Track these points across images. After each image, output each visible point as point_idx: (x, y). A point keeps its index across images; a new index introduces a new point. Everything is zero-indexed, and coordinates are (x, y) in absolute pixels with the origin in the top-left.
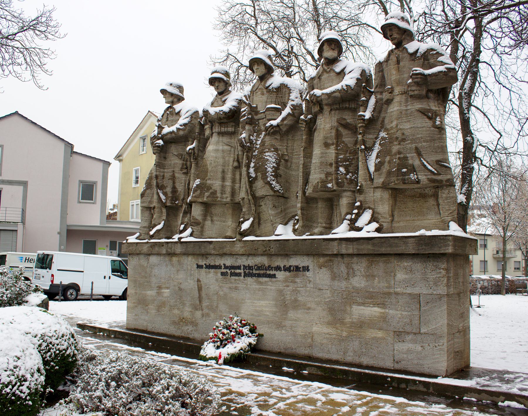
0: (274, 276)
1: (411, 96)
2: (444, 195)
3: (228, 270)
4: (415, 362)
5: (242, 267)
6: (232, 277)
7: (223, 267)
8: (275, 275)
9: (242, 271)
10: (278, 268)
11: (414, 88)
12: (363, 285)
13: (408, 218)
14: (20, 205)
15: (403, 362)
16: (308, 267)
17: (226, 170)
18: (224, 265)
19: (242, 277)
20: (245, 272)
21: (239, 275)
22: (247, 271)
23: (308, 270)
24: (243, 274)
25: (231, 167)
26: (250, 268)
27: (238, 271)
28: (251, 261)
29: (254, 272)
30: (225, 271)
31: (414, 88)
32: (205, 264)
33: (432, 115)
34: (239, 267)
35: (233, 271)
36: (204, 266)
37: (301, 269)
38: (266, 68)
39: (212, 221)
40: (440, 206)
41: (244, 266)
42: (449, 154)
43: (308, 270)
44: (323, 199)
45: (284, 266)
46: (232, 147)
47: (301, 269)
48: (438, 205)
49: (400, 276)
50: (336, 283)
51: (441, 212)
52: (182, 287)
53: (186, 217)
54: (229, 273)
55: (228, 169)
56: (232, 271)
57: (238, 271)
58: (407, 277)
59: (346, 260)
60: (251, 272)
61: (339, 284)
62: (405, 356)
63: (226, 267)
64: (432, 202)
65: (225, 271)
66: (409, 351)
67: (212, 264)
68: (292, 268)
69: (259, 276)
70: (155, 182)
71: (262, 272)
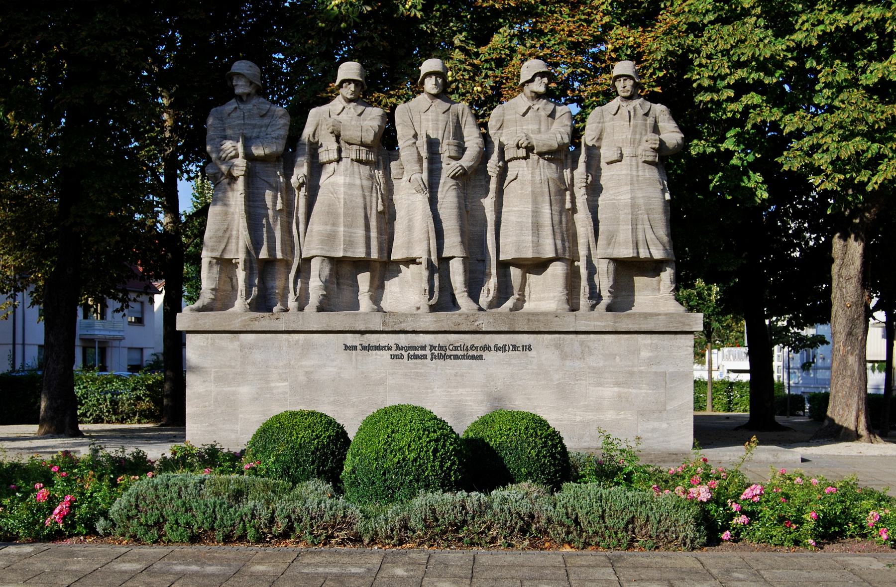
0: (480, 357)
5: (428, 348)
9: (427, 352)
12: (601, 365)
14: (542, 329)
16: (530, 346)
21: (424, 357)
24: (429, 357)
26: (441, 348)
29: (448, 353)
30: (398, 352)
32: (361, 345)
33: (452, 82)
34: (423, 348)
36: (359, 347)
37: (520, 349)
42: (363, 107)
47: (520, 349)
50: (568, 363)
56: (414, 353)
57: (420, 353)
58: (651, 354)
60: (443, 353)
62: (650, 435)
63: (398, 347)
65: (398, 352)
66: (654, 430)
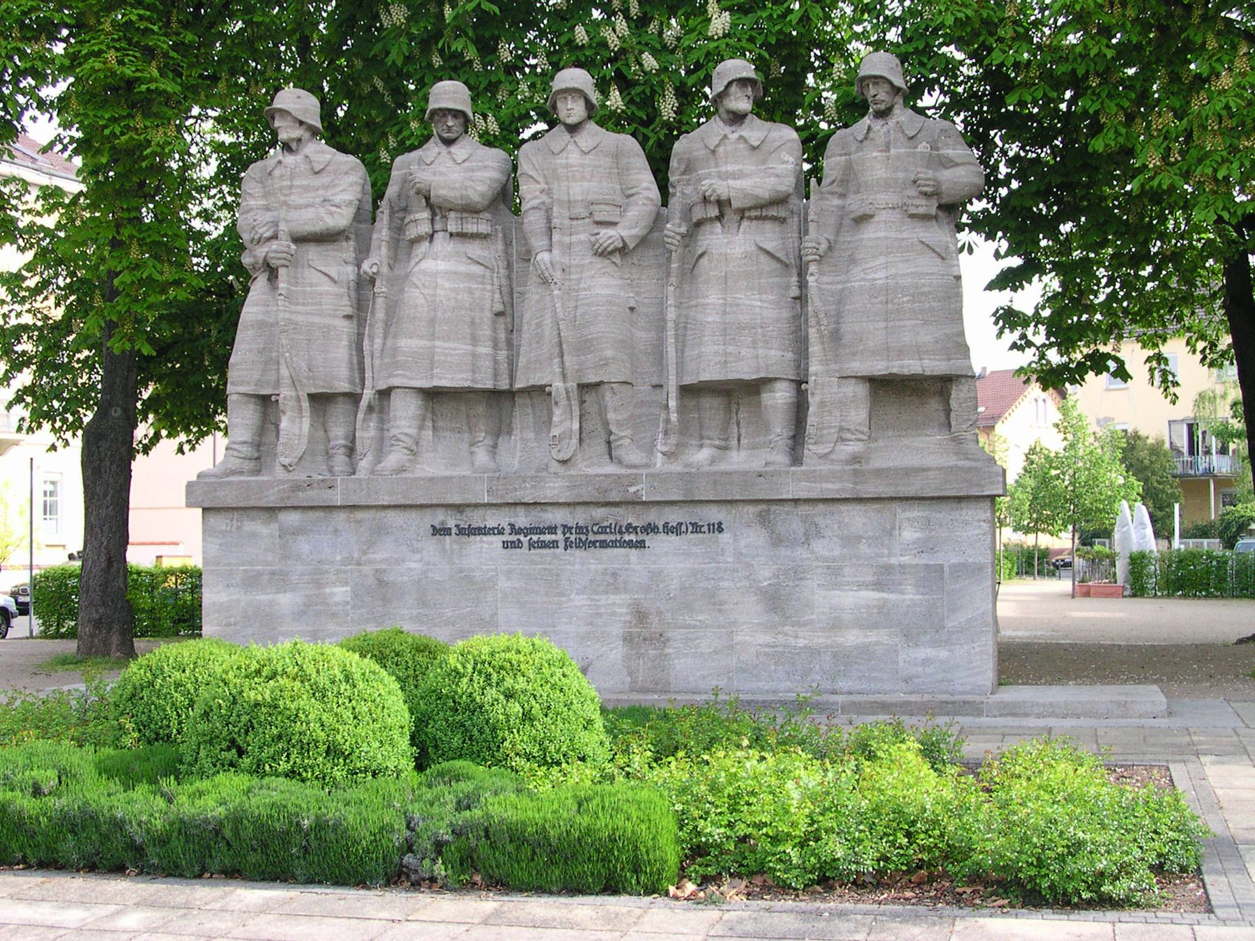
0: (641, 545)
1: (912, 216)
2: (962, 395)
3: (522, 537)
4: (939, 677)
6: (533, 551)
7: (508, 530)
8: (644, 541)
9: (559, 536)
10: (651, 529)
11: (917, 202)
13: (890, 433)
15: (916, 681)
16: (720, 524)
17: (477, 320)
18: (512, 526)
19: (560, 550)
20: (567, 540)
21: (554, 544)
22: (573, 538)
23: (721, 530)
24: (561, 544)
25: (488, 314)
26: (580, 530)
27: (548, 537)
28: (580, 517)
29: (592, 537)
30: (514, 538)
31: (917, 202)
32: (457, 526)
34: (552, 530)
35: (535, 538)
36: (454, 530)
38: (587, 108)
39: (435, 428)
40: (953, 414)
41: (565, 526)
43: (721, 530)
44: (862, 378)
45: (666, 525)
46: (486, 267)
47: (705, 529)
48: (948, 411)
49: (909, 535)
51: (953, 423)
52: (389, 578)
53: (370, 420)
54: (526, 544)
55: (481, 318)
57: (548, 537)
59: (804, 509)
61: (789, 553)
63: (514, 530)
64: (934, 405)
65: (514, 538)
66: (926, 662)
67: (474, 525)
68: (683, 528)
69: (604, 545)
70: (94, 817)
71: (609, 538)
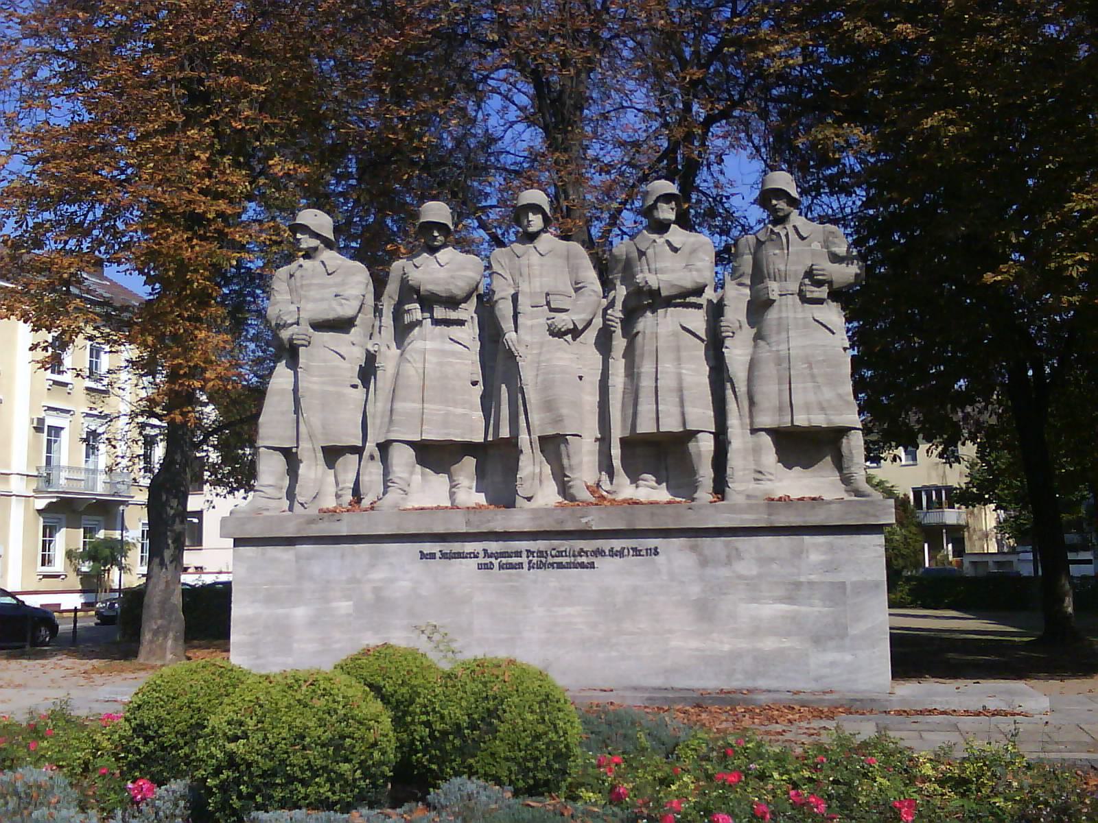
9: (524, 560)
47: (644, 552)
65: (487, 560)
